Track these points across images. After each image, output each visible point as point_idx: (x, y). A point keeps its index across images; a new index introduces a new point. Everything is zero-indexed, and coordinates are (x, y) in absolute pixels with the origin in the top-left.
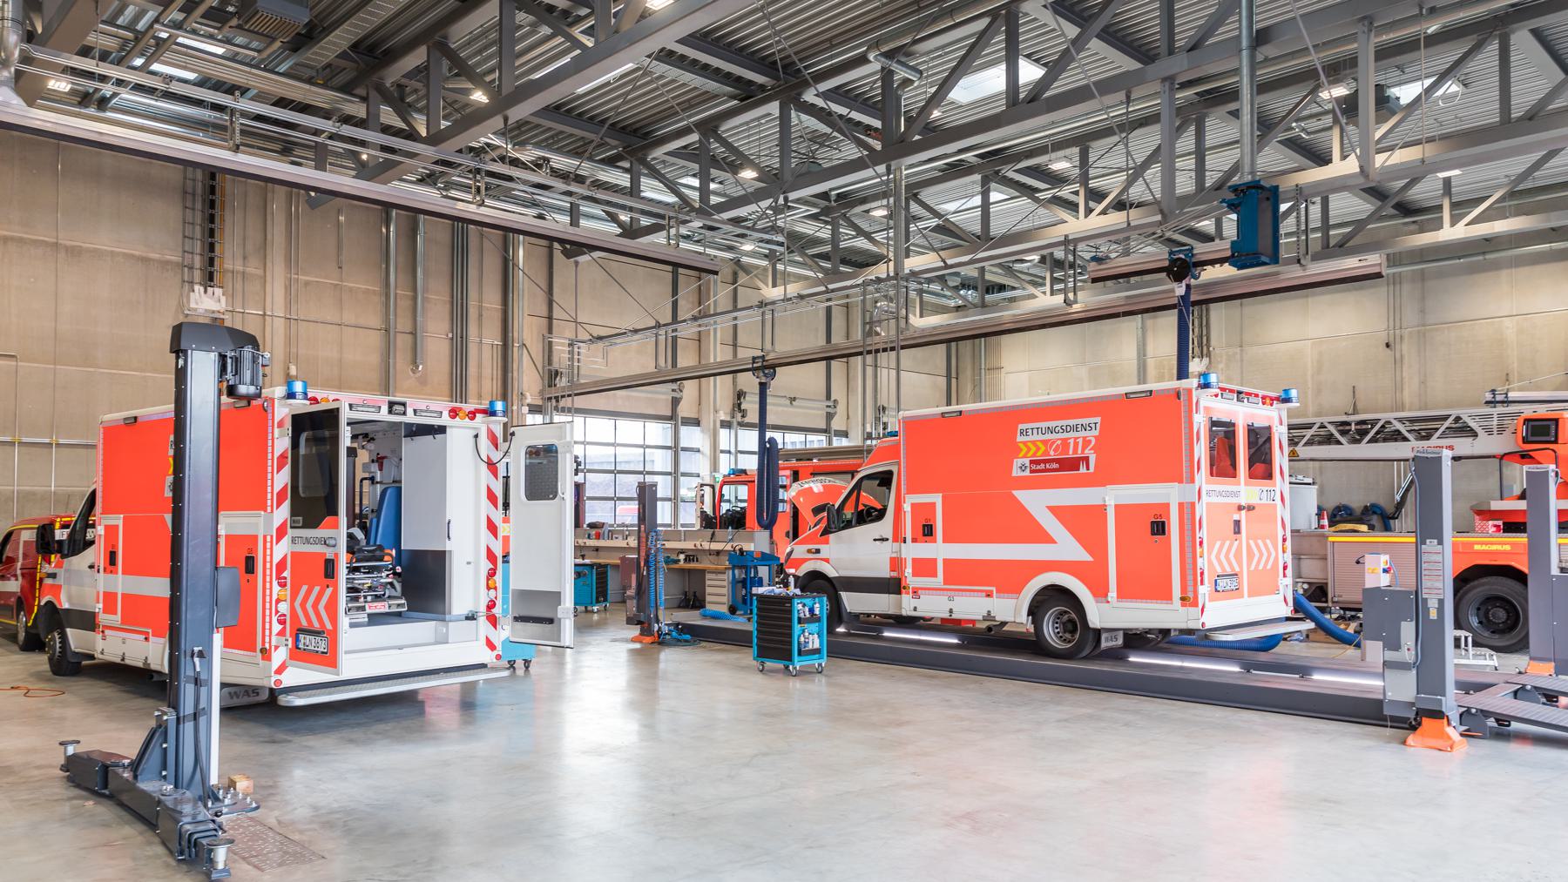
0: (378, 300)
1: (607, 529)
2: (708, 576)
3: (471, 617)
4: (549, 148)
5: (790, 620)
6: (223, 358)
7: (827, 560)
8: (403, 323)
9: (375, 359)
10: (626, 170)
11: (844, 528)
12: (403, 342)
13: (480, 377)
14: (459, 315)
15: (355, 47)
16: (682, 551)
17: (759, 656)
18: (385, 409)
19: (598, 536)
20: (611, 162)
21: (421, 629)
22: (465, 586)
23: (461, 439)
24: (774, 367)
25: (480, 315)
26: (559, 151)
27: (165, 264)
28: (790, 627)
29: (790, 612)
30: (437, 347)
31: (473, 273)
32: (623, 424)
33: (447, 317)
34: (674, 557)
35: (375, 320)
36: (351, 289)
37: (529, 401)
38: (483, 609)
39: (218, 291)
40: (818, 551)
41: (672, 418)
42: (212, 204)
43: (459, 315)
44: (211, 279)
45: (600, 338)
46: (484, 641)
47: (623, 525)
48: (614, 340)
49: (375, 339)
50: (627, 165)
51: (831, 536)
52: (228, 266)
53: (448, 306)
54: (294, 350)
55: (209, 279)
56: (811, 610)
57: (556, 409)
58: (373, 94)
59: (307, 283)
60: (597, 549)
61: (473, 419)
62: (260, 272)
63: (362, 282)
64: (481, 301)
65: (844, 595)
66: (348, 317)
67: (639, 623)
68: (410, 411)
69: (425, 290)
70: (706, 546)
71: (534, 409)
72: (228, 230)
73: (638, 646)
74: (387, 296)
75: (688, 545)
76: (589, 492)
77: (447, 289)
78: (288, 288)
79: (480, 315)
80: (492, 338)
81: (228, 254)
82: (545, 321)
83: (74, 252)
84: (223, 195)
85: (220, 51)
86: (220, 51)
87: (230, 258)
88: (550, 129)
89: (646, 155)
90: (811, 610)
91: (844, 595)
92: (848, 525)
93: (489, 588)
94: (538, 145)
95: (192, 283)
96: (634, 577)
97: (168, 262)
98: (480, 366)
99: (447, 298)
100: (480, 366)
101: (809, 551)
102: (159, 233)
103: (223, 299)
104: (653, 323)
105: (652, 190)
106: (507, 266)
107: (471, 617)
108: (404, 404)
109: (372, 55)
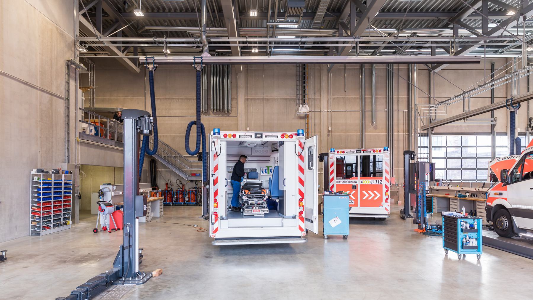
0: (359, 101)
1: (441, 181)
2: (477, 204)
3: (294, 217)
4: (416, 28)
5: (456, 229)
6: (135, 120)
7: (506, 199)
8: (368, 108)
9: (358, 122)
10: (452, 28)
11: (515, 182)
12: (368, 114)
13: (398, 124)
14: (389, 102)
15: (328, 10)
16: (468, 192)
17: (445, 246)
18: (253, 136)
19: (438, 185)
20: (446, 26)
21: (275, 221)
22: (291, 206)
23: (290, 148)
24: (519, 103)
25: (398, 101)
26: (421, 28)
27: (291, 99)
28: (456, 234)
29: (456, 225)
30: (381, 116)
31: (395, 85)
32: (479, 138)
33: (385, 103)
34: (463, 194)
35: (358, 108)
36: (349, 98)
37: (419, 131)
38: (297, 214)
39: (307, 105)
40: (501, 194)
41: (492, 133)
42: (304, 78)
43: (389, 102)
44: (304, 102)
45: (442, 102)
46: (298, 227)
47: (450, 180)
48: (447, 102)
49: (358, 114)
50: (452, 26)
51: (508, 186)
52: (310, 97)
53: (385, 99)
54: (330, 122)
55: (304, 102)
56: (472, 226)
57: (432, 134)
58: (340, 27)
59: (334, 99)
60: (438, 190)
61: (292, 137)
62: (319, 97)
63: (354, 95)
64: (398, 95)
65: (515, 218)
66: (349, 108)
67: (417, 223)
68: (264, 137)
69: (376, 94)
70: (480, 189)
71: (421, 135)
72: (309, 85)
73: (415, 233)
74: (361, 99)
75: (473, 189)
76: (436, 166)
77: (385, 93)
78: (328, 101)
79: (398, 101)
80: (403, 108)
81: (309, 93)
82: (427, 99)
83: (268, 100)
84: (308, 74)
85: (296, 26)
86: (296, 26)
87: (310, 95)
88: (418, 20)
89: (460, 19)
90: (472, 226)
91: (515, 218)
92: (518, 180)
93: (300, 206)
94: (410, 28)
95: (299, 104)
96: (415, 203)
97: (293, 99)
98: (398, 120)
99: (385, 96)
100: (398, 120)
101: (496, 194)
102: (286, 91)
103: (308, 108)
104: (462, 92)
105: (463, 32)
106: (409, 79)
107: (294, 217)
108: (261, 134)
109: (335, 11)
